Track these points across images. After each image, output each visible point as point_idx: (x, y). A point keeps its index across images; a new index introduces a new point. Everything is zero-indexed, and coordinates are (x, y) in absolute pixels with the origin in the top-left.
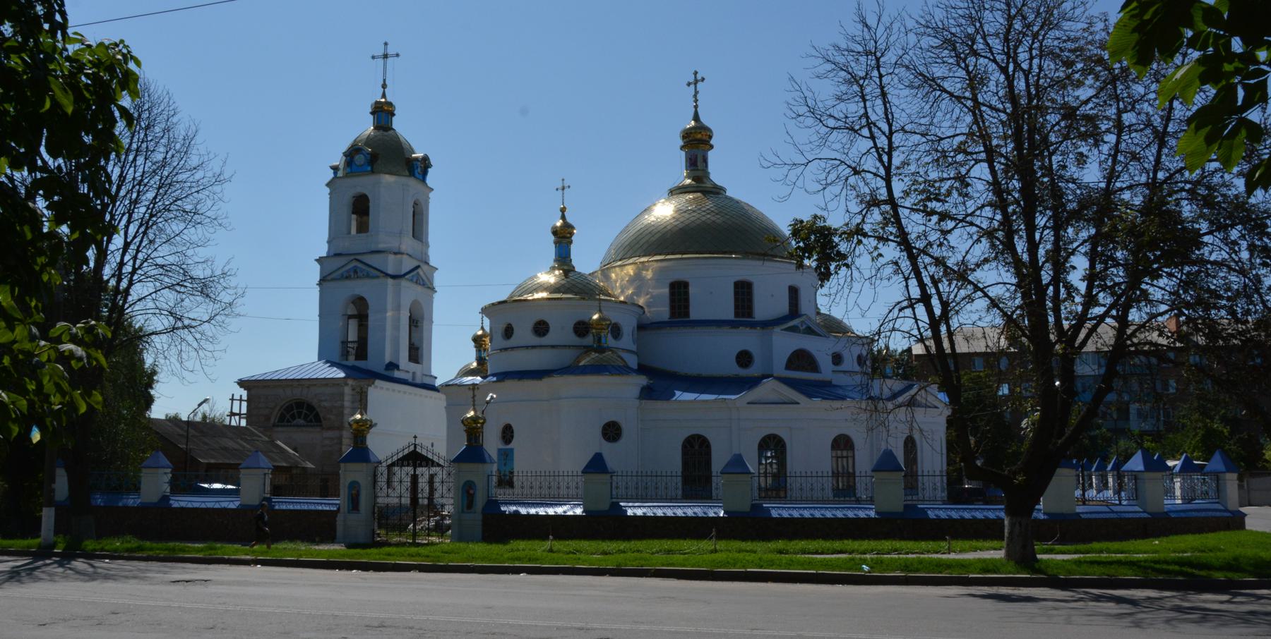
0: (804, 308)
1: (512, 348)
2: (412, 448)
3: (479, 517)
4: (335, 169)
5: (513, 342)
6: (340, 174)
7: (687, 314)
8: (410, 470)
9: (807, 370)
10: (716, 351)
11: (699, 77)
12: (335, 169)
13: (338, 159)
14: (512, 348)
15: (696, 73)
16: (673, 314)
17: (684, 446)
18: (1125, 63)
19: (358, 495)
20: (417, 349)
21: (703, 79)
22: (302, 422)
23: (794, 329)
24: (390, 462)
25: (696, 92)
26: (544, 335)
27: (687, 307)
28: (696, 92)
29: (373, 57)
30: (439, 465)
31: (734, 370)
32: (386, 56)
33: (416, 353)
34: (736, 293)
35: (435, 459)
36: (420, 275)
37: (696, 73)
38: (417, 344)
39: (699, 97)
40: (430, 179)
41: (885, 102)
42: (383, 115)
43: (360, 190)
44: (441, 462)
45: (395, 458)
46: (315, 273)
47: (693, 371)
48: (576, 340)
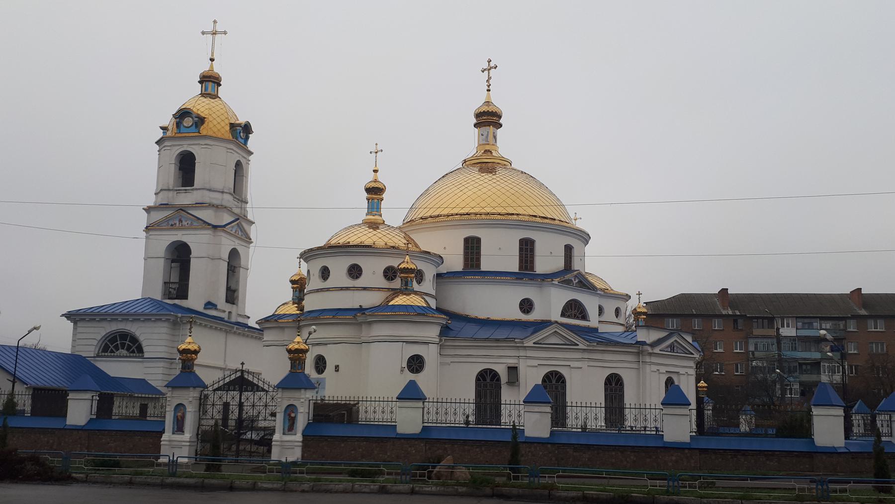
0: (576, 266)
1: (328, 289)
2: (239, 374)
3: (299, 437)
4: (164, 129)
5: (329, 284)
6: (169, 134)
7: (479, 266)
8: (236, 394)
9: (578, 318)
10: (498, 302)
11: (492, 64)
12: (164, 129)
13: (167, 119)
14: (328, 289)
15: (489, 61)
16: (466, 265)
17: (478, 379)
18: (828, 348)
19: (183, 417)
20: (234, 291)
21: (496, 67)
22: (124, 352)
23: (568, 282)
24: (216, 386)
25: (490, 78)
26: (357, 278)
27: (479, 260)
28: (490, 78)
29: (203, 33)
30: (263, 390)
31: (517, 315)
32: (214, 33)
33: (232, 296)
34: (521, 250)
35: (261, 384)
36: (239, 226)
37: (489, 61)
38: (233, 287)
39: (491, 82)
40: (251, 144)
41: (345, 492)
42: (210, 85)
43: (185, 148)
44: (266, 387)
45: (221, 383)
46: (143, 219)
47: (482, 315)
48: (384, 283)
